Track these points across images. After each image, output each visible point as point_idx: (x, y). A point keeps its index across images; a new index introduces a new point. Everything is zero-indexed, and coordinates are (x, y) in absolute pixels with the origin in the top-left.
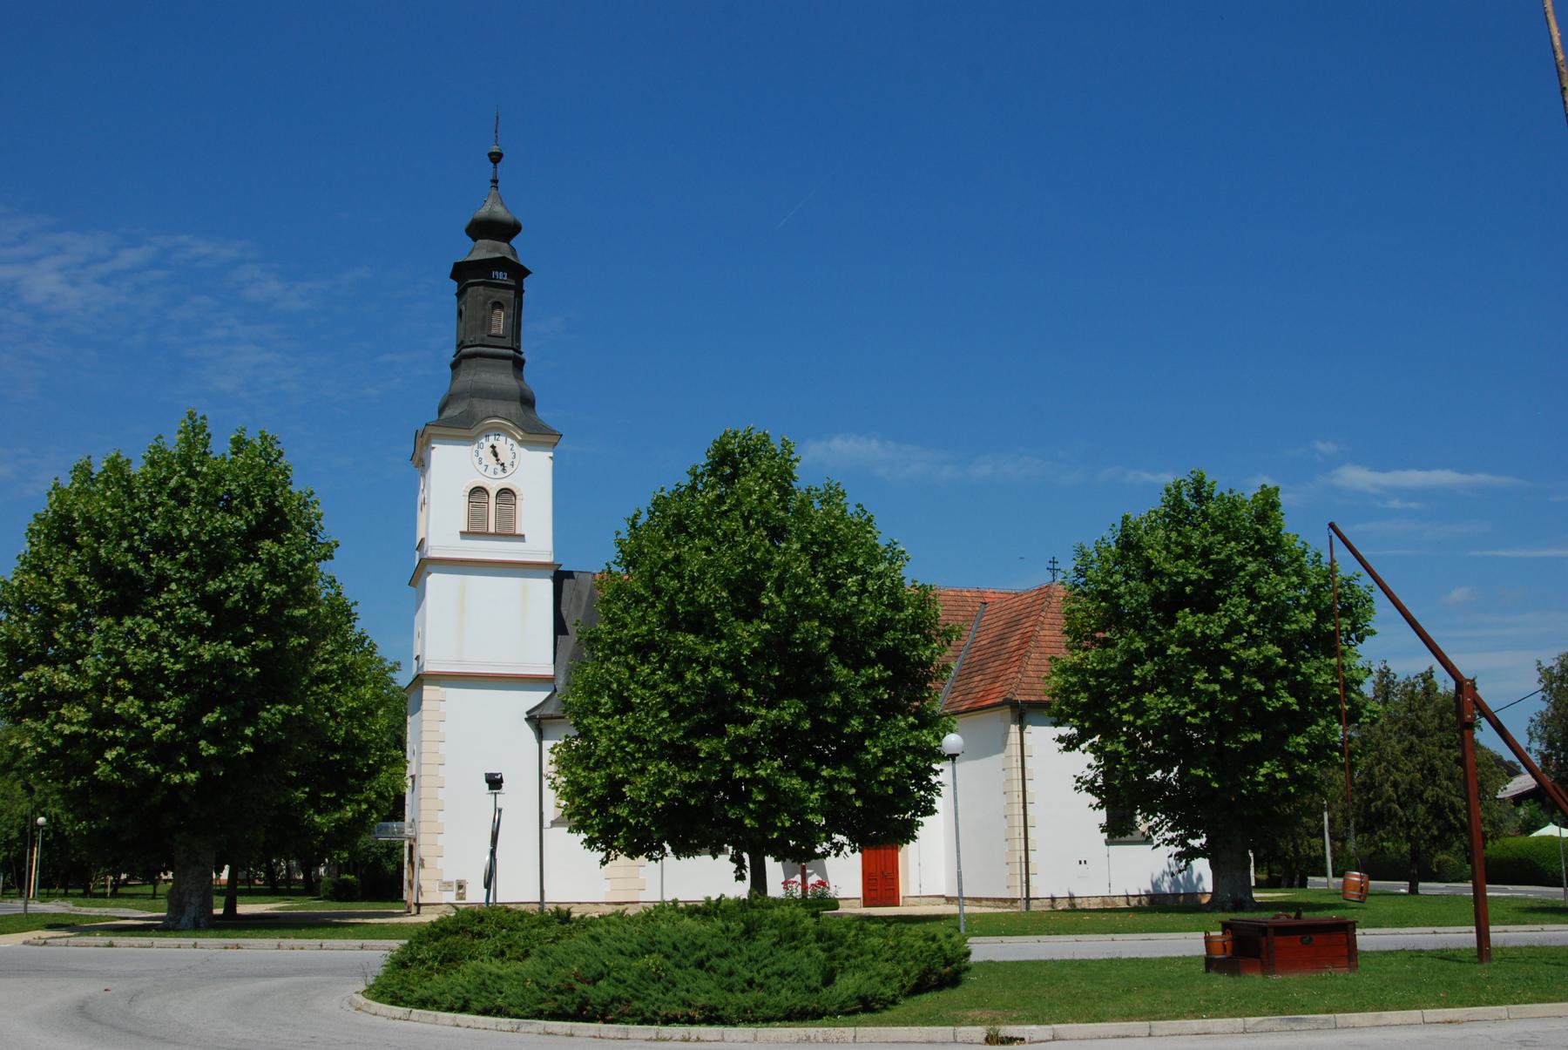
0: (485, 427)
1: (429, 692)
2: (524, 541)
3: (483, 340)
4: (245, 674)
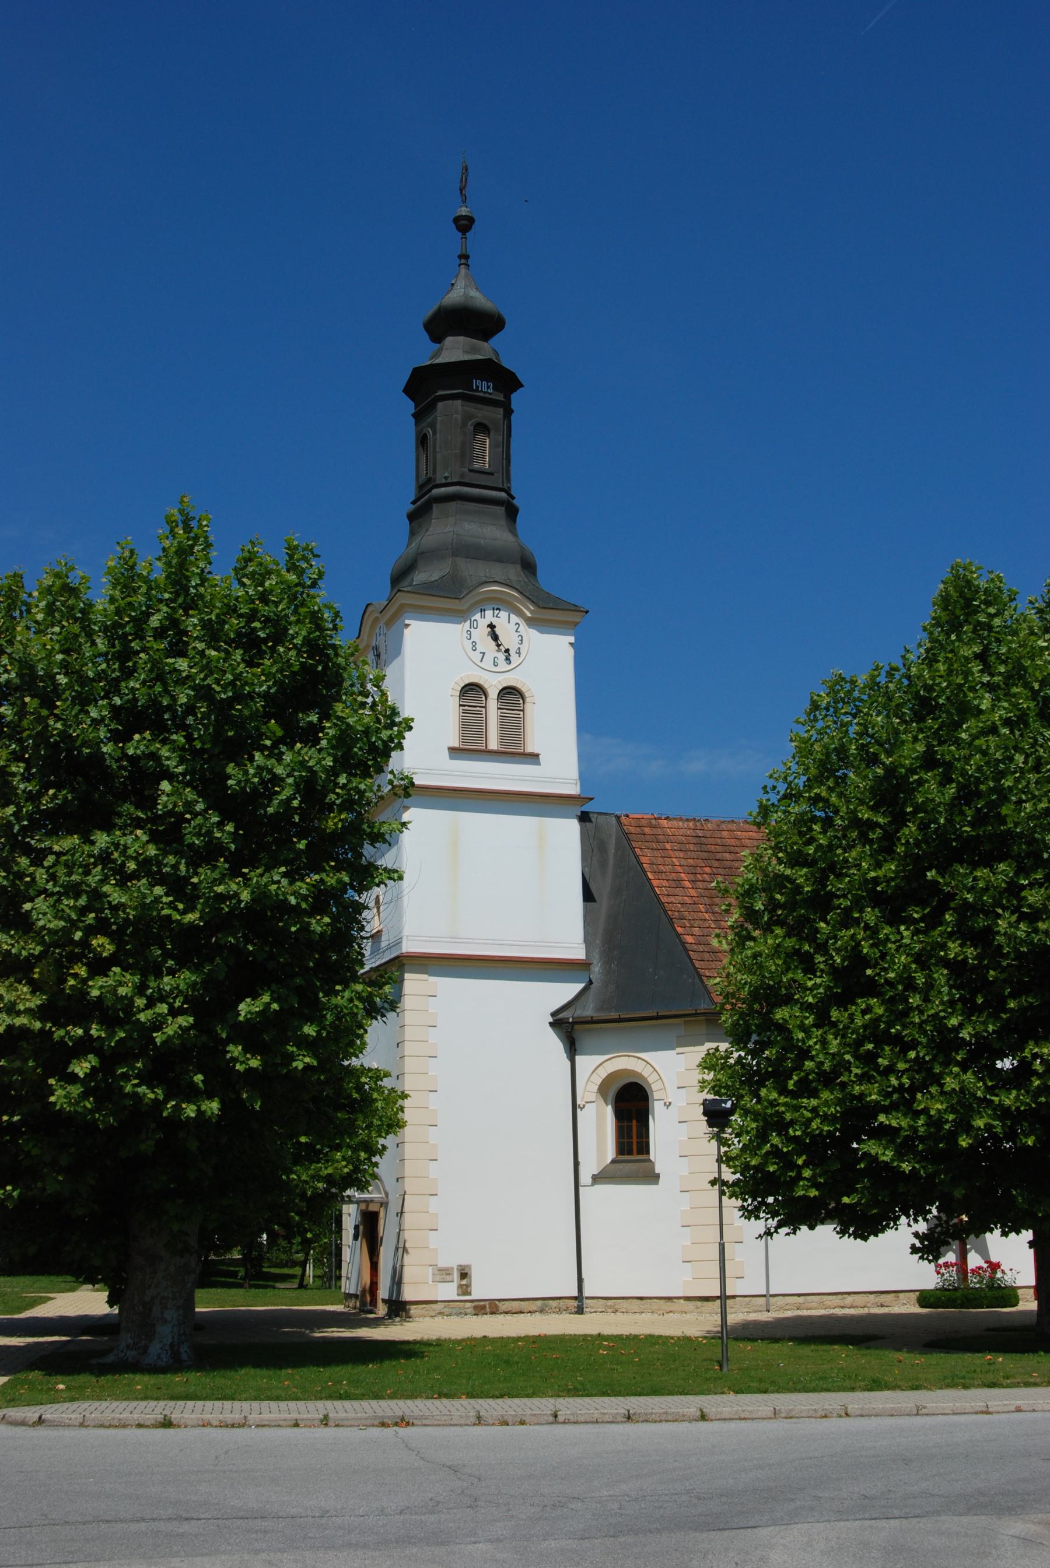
0: (482, 597)
1: (413, 983)
2: (539, 764)
3: (462, 475)
4: (306, 928)
